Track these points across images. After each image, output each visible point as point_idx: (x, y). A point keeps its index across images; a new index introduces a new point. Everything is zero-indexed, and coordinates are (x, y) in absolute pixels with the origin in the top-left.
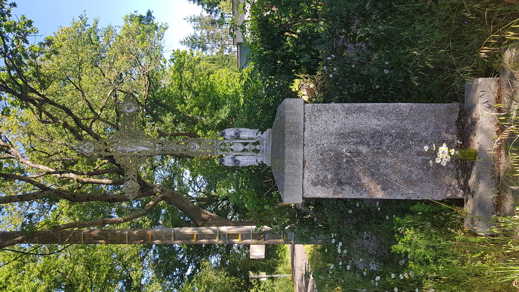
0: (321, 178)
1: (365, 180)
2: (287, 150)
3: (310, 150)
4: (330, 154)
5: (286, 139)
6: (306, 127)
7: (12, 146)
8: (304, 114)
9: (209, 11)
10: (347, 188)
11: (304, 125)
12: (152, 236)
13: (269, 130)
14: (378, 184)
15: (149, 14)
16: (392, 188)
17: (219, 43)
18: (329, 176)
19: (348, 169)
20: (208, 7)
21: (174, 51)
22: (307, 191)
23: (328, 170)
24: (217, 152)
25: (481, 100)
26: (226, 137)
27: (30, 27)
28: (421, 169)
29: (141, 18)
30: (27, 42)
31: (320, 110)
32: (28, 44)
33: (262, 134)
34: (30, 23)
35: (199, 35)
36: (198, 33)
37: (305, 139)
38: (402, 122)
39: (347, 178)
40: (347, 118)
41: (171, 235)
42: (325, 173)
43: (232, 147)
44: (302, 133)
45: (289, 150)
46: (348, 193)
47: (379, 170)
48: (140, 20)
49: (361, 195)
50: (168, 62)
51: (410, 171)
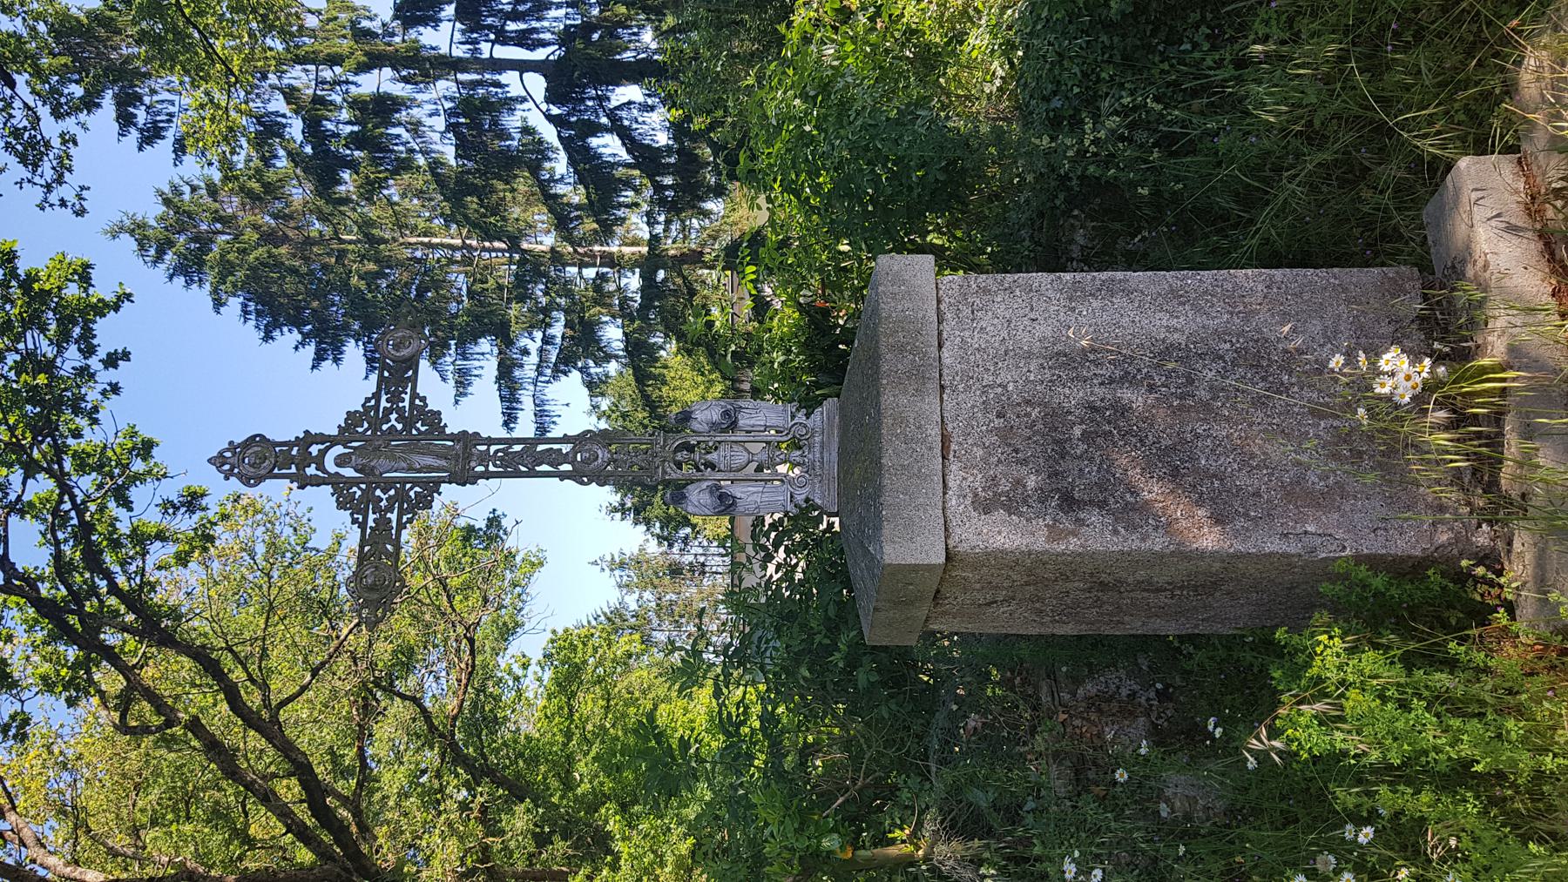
0: (1005, 486)
1: (1153, 491)
2: (887, 399)
3: (964, 403)
4: (1028, 415)
5: (885, 368)
6: (945, 335)
7: (14, 808)
8: (939, 302)
10: (1094, 517)
11: (940, 334)
13: (830, 404)
14: (1199, 503)
15: (494, 521)
16: (1246, 515)
18: (1032, 482)
19: (1091, 460)
21: (554, 632)
22: (959, 531)
23: (1024, 462)
24: (665, 472)
25: (1480, 214)
26: (695, 425)
27: (144, 460)
28: (1335, 456)
29: (470, 531)
30: (127, 504)
31: (986, 291)
32: (131, 509)
33: (808, 416)
35: (633, 606)
36: (631, 602)
37: (945, 371)
38: (1246, 320)
39: (1090, 486)
40: (1073, 310)
43: (713, 457)
44: (934, 349)
45: (892, 399)
46: (1097, 537)
47: (1193, 459)
48: (466, 539)
49: (1143, 540)
51: (1299, 463)
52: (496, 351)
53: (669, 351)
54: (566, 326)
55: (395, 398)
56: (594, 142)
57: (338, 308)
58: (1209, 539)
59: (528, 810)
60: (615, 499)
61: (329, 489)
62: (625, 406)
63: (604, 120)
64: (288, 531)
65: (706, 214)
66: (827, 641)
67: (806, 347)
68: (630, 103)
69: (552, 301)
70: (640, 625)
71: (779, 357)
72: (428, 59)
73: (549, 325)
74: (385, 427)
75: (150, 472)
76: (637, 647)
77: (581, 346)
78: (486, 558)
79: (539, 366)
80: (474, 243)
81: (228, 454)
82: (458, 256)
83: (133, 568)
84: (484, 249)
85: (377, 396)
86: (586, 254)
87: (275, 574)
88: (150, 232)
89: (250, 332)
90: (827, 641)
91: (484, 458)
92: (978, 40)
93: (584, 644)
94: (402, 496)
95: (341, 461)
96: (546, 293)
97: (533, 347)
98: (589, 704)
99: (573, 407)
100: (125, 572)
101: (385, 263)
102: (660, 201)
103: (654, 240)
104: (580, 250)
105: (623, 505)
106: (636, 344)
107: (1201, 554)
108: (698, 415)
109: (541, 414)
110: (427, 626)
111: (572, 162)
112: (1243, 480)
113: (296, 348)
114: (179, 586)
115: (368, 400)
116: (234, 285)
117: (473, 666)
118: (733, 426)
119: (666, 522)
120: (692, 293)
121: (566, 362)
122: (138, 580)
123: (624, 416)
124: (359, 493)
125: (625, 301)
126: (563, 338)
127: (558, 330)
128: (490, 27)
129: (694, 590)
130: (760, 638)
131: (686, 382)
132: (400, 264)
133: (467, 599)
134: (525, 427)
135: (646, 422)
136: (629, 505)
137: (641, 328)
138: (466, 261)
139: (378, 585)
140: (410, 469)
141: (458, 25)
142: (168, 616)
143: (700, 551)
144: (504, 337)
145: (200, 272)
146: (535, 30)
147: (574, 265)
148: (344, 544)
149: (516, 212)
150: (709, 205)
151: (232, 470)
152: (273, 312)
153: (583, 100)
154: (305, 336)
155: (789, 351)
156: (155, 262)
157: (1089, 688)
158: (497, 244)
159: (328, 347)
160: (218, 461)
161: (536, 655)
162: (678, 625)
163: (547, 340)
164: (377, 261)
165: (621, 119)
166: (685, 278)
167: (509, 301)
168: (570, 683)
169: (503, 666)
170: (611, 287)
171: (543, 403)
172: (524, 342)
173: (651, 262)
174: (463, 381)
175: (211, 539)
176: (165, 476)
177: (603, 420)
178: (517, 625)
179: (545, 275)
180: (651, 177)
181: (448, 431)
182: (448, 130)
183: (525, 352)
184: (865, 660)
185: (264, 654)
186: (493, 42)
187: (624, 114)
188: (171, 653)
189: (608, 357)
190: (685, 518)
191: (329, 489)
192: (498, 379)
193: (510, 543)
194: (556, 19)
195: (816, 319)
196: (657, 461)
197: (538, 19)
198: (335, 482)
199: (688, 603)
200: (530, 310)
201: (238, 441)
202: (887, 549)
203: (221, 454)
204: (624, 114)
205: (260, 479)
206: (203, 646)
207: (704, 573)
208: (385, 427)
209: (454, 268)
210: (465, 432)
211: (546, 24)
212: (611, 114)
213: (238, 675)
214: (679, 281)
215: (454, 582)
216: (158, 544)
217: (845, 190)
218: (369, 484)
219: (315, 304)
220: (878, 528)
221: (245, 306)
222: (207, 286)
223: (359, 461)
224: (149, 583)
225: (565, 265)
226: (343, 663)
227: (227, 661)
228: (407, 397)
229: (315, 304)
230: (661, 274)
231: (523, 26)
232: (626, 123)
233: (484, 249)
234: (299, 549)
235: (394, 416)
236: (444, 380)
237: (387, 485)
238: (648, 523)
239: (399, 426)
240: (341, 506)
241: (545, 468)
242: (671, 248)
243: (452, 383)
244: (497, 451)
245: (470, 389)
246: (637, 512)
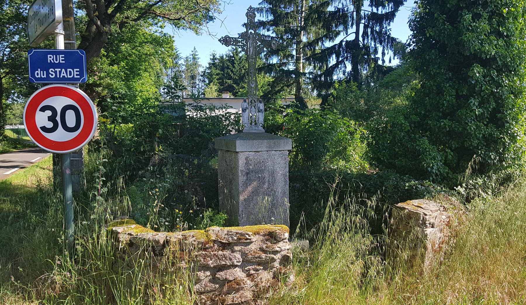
1: (250, 189)
2: (265, 141)
9: (204, 74)
12: (69, 21)
15: (211, 19)
18: (251, 167)
20: (208, 73)
21: (173, 37)
29: (208, 10)
35: (180, 62)
36: (181, 62)
41: (70, 40)
42: (253, 165)
43: (253, 107)
46: (241, 179)
48: (206, 9)
50: (160, 29)
56: (334, 56)
58: (241, 198)
59: (116, 31)
63: (340, 59)
65: (313, 91)
67: (273, 125)
68: (346, 67)
69: (285, 41)
71: (271, 118)
72: (359, 4)
82: (299, 8)
92: (342, 163)
93: (169, 48)
94: (244, 45)
98: (148, 49)
102: (317, 76)
103: (304, 74)
104: (301, 50)
107: (239, 197)
111: (328, 49)
112: (252, 204)
118: (259, 112)
119: (210, 74)
120: (288, 86)
125: (285, 64)
128: (369, 23)
137: (276, 70)
141: (370, 13)
143: (200, 86)
146: (368, 37)
149: (313, 29)
150: (315, 92)
153: (346, 52)
155: (272, 120)
157: (199, 189)
158: (303, 23)
161: (165, 31)
165: (341, 64)
166: (293, 84)
168: (156, 42)
170: (290, 59)
173: (297, 73)
178: (178, 27)
179: (293, 39)
180: (323, 73)
182: (338, 9)
186: (364, 24)
187: (343, 65)
189: (267, 59)
190: (212, 81)
194: (371, 44)
197: (371, 39)
202: (239, 141)
204: (343, 65)
205: (247, 16)
211: (370, 41)
212: (343, 61)
214: (292, 82)
217: (311, 134)
231: (369, 33)
232: (340, 66)
233: (301, 18)
236: (259, 4)
237: (247, 43)
238: (209, 68)
242: (302, 79)
243: (258, 6)
246: (213, 64)
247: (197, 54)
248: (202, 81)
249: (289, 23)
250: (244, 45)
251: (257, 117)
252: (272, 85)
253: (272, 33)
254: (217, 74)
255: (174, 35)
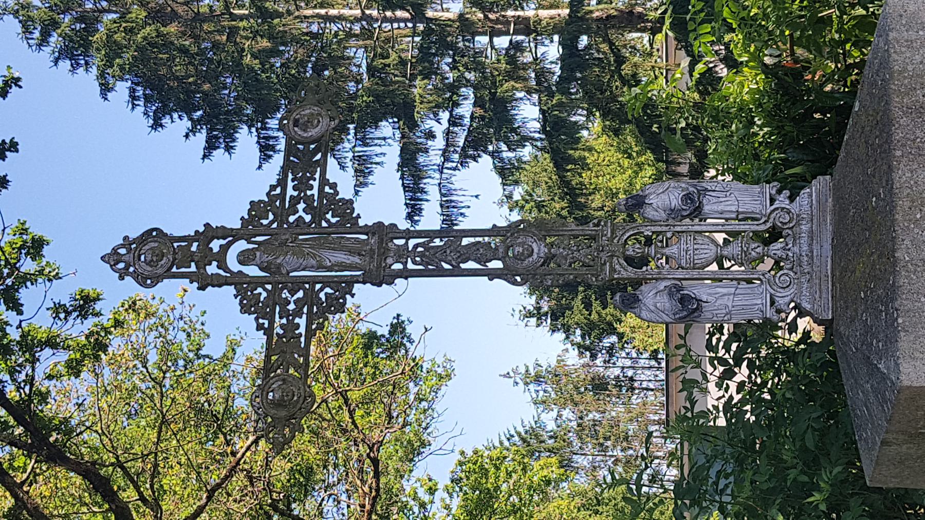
2: (902, 176)
5: (898, 135)
9: (587, 348)
13: (820, 184)
15: (398, 327)
17: (618, 453)
21: (462, 453)
24: (613, 270)
26: (650, 213)
27: (33, 259)
29: (371, 338)
32: (20, 313)
33: (792, 199)
34: (36, 247)
35: (551, 426)
36: (549, 420)
48: (367, 347)
50: (440, 494)
52: (398, 135)
53: (592, 131)
54: (475, 104)
55: (302, 185)
57: (230, 90)
60: (530, 302)
61: (231, 290)
62: (541, 194)
64: (182, 336)
66: (805, 479)
70: (561, 450)
73: (457, 104)
74: (292, 219)
75: (41, 272)
76: (555, 472)
77: (493, 127)
78: (386, 366)
79: (445, 151)
80: (375, 13)
81: (123, 251)
82: (357, 28)
83: (22, 377)
84: (385, 20)
85: (282, 183)
86: (497, 21)
87: (167, 382)
88: (34, 13)
89: (139, 118)
90: (805, 479)
91: (402, 254)
93: (497, 468)
94: (311, 298)
95: (244, 258)
96: (453, 68)
97: (439, 129)
99: (483, 197)
100: (14, 380)
101: (279, 39)
104: (492, 16)
105: (539, 309)
106: (556, 123)
108: (653, 200)
109: (448, 205)
110: (328, 444)
113: (187, 136)
114: (70, 399)
115: (273, 188)
116: (122, 68)
117: (378, 490)
118: (697, 212)
119: (589, 328)
120: (620, 60)
121: (476, 145)
122: (27, 389)
123: (540, 206)
124: (264, 294)
125: (542, 74)
126: (472, 118)
127: (466, 109)
129: (621, 409)
130: (719, 472)
131: (610, 163)
132: (296, 40)
133: (369, 414)
134: (431, 219)
135: (564, 213)
136: (545, 309)
137: (560, 104)
138: (367, 34)
139: (284, 402)
140: (320, 267)
142: (57, 429)
143: (628, 363)
144: (408, 122)
145: (86, 54)
147: (484, 34)
148: (239, 351)
151: (127, 268)
152: (163, 96)
154: (196, 123)
156: (40, 46)
158: (400, 13)
159: (220, 137)
160: (112, 258)
161: (443, 480)
162: (603, 449)
163: (455, 121)
164: (271, 38)
166: (611, 44)
167: (413, 77)
169: (408, 490)
170: (527, 58)
171: (449, 193)
172: (430, 124)
174: (363, 170)
175: (104, 348)
176: (57, 277)
177: (516, 210)
178: (423, 444)
179: (453, 46)
181: (361, 223)
183: (431, 135)
184: (853, 502)
185: (155, 473)
188: (61, 472)
189: (524, 140)
190: (610, 324)
191: (231, 290)
192: (401, 166)
193: (416, 351)
195: (786, 82)
196: (604, 256)
198: (239, 282)
199: (615, 423)
200: (436, 87)
201: (134, 234)
203: (115, 250)
205: (156, 280)
206: (94, 463)
207: (632, 389)
208: (292, 219)
209: (353, 42)
210: (380, 224)
213: (129, 495)
214: (605, 47)
215: (355, 395)
216: (48, 351)
218: (275, 284)
219: (206, 87)
220: (892, 340)
221: (132, 91)
222: (94, 70)
223: (265, 258)
224: (40, 393)
225: (474, 34)
226: (239, 480)
227: (119, 480)
228: (316, 184)
229: (206, 87)
230: (584, 41)
233: (385, 20)
234: (191, 355)
235: (301, 206)
236: (343, 167)
237: (297, 285)
238: (567, 330)
239: (308, 218)
240: (245, 309)
241: (471, 265)
243: (351, 171)
244: (416, 246)
245: (371, 179)
246: (555, 318)
247: (522, 370)
248: (611, 355)
249: (403, 62)
250: (311, 298)
251: (735, 226)
252: (616, 118)
253: (438, 121)
254: (588, 306)
255: (457, 450)
